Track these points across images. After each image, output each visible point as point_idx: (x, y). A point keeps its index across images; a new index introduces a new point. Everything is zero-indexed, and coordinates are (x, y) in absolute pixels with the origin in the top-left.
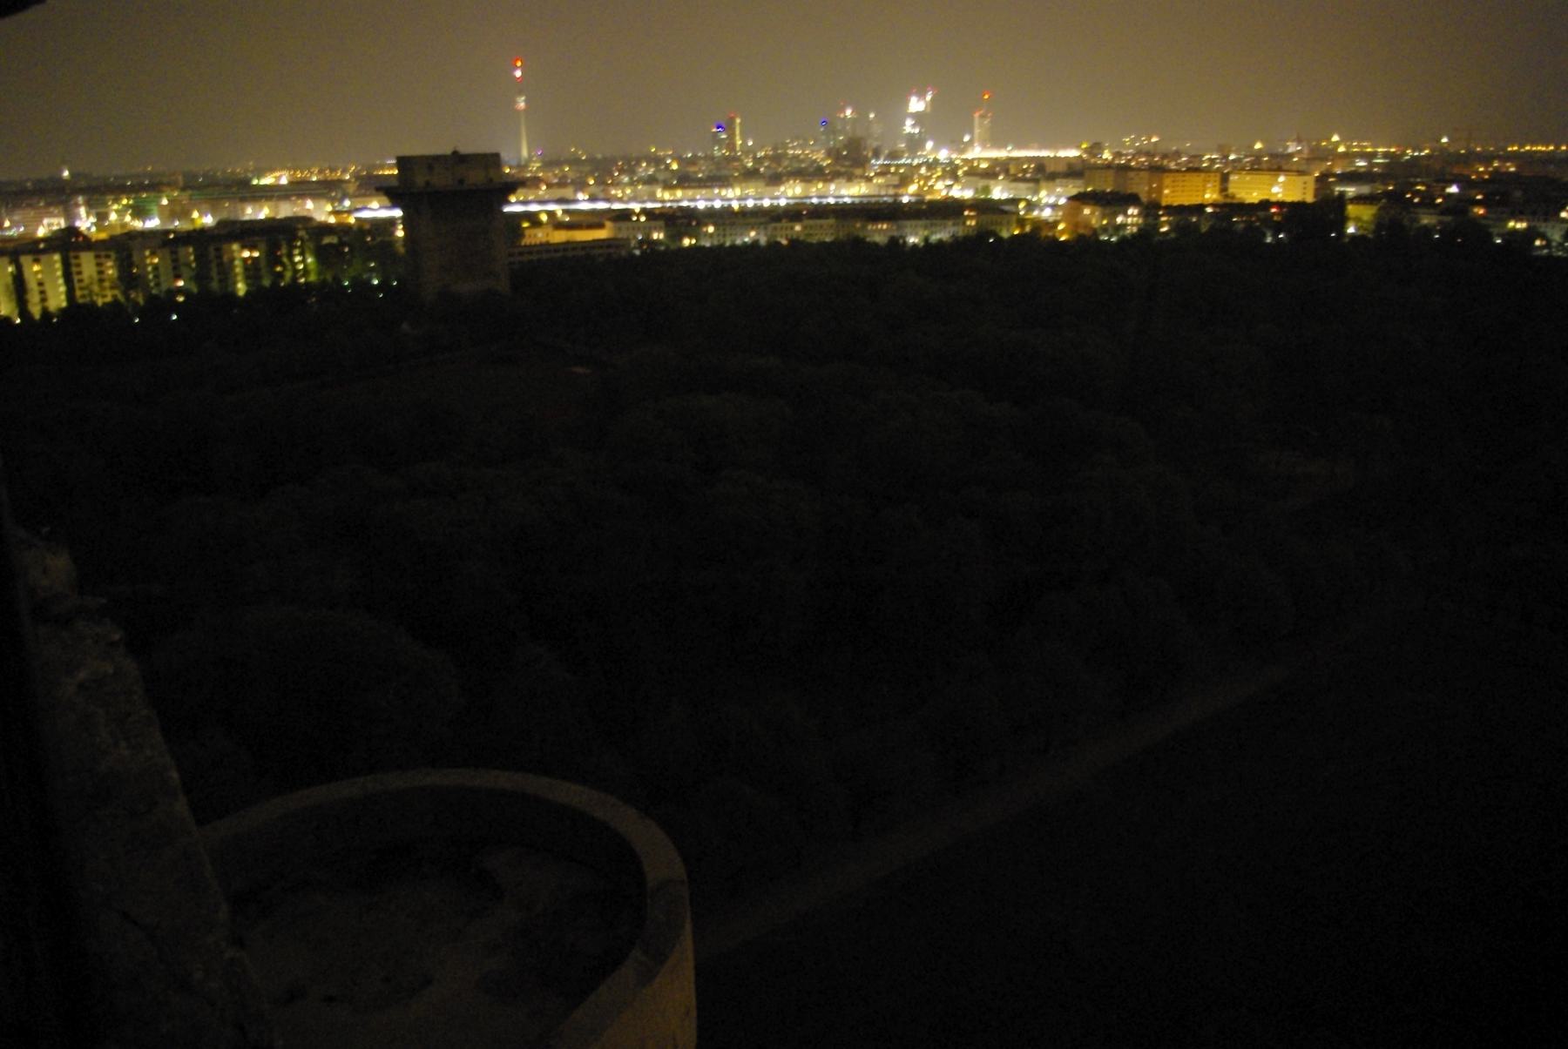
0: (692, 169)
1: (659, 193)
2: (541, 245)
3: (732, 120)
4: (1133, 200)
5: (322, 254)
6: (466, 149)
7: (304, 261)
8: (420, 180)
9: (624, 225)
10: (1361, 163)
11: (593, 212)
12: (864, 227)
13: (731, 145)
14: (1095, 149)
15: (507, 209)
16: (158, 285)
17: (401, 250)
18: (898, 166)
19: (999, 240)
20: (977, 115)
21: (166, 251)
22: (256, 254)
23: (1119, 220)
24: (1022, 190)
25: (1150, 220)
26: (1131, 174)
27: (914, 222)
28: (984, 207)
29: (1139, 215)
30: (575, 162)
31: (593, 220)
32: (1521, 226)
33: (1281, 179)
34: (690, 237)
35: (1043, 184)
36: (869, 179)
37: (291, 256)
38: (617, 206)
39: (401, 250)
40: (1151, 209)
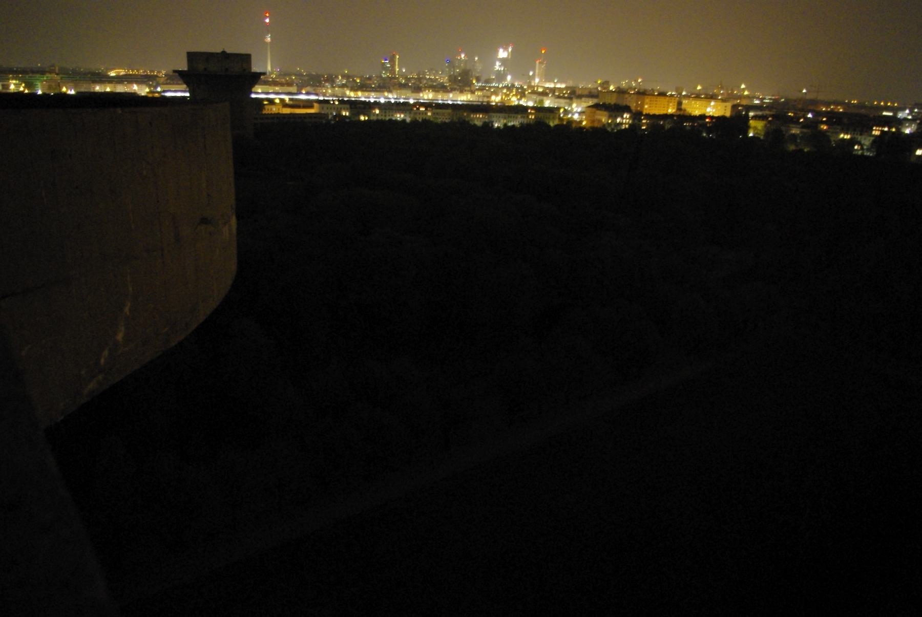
1: (348, 92)
3: (394, 56)
4: (627, 109)
6: (229, 51)
8: (201, 67)
9: (326, 106)
10: (757, 102)
12: (468, 116)
13: (392, 71)
14: (606, 84)
15: (253, 96)
18: (490, 87)
20: (537, 62)
23: (618, 120)
24: (561, 103)
27: (498, 115)
28: (539, 109)
29: (630, 118)
30: (299, 75)
31: (308, 104)
32: (847, 137)
33: (712, 103)
34: (364, 115)
35: (574, 100)
36: (473, 92)
38: (321, 98)
40: (637, 115)
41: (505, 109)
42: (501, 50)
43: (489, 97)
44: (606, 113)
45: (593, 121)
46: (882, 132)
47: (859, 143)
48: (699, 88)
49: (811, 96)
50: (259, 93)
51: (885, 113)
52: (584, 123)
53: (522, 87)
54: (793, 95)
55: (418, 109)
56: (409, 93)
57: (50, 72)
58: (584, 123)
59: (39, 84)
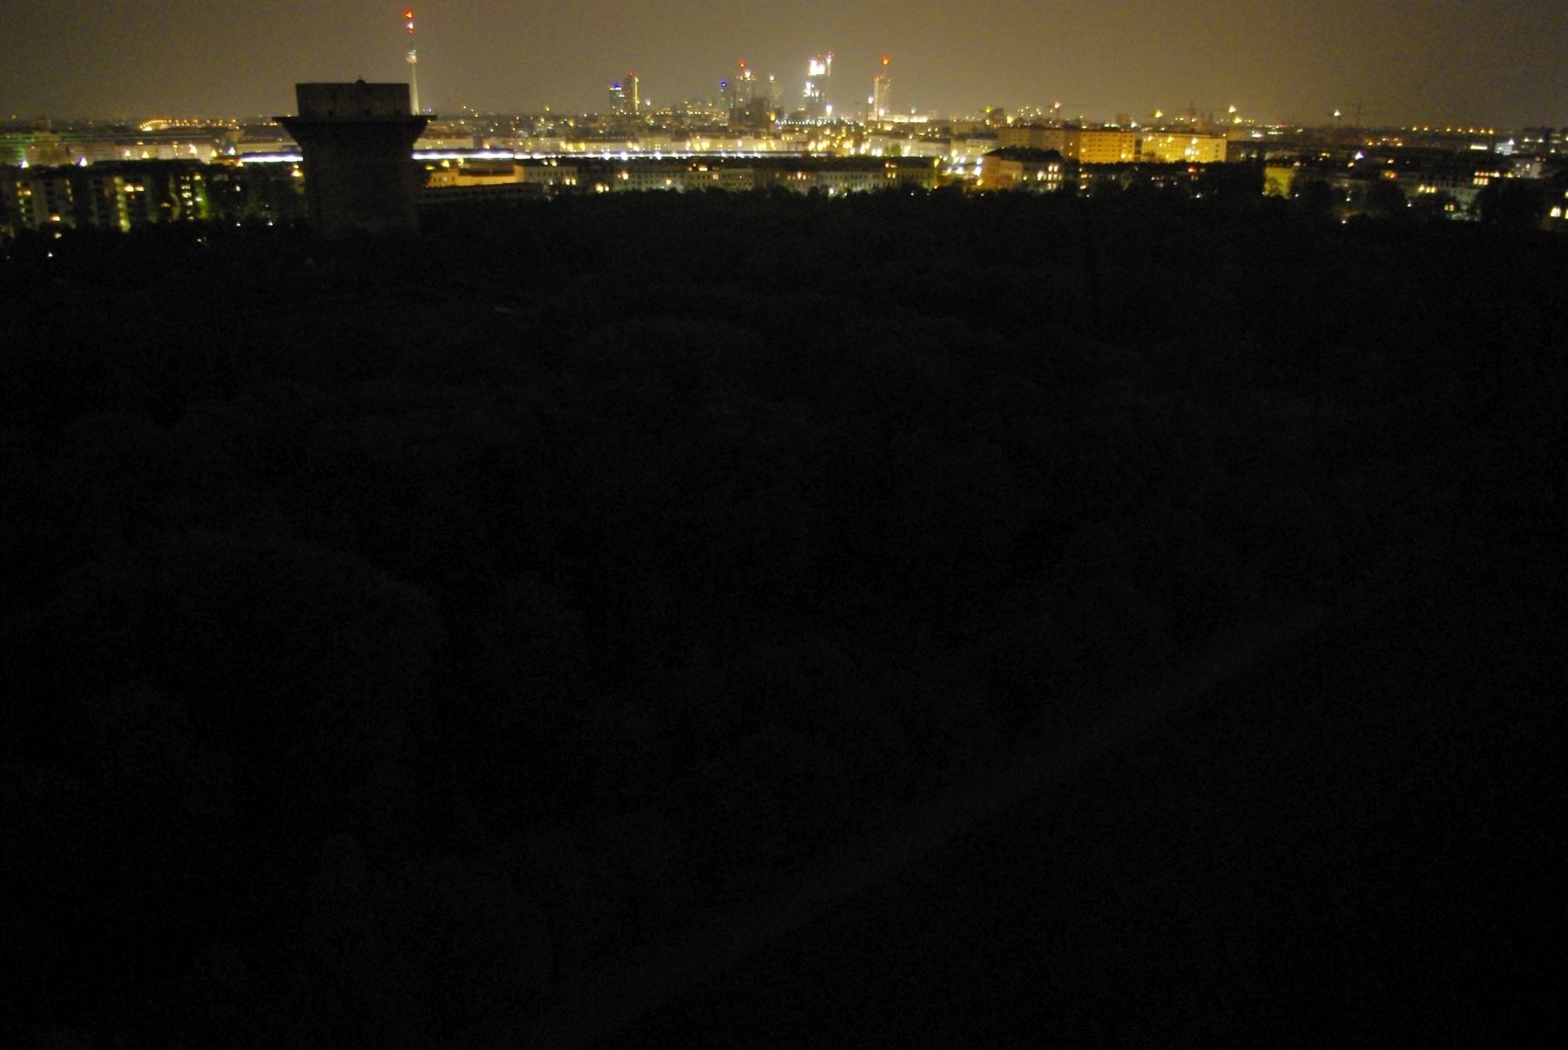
0: (592, 125)
1: (563, 145)
2: (448, 188)
4: (1053, 156)
5: (213, 190)
6: (371, 79)
7: (192, 198)
9: (534, 169)
10: (1257, 135)
11: (496, 161)
12: (783, 177)
13: (629, 105)
14: (998, 114)
15: (417, 157)
16: (31, 219)
17: (301, 191)
18: (802, 127)
19: (922, 192)
20: (877, 80)
21: (41, 183)
22: (141, 189)
23: (1040, 176)
24: (930, 150)
25: (1071, 176)
26: (1048, 133)
27: (834, 174)
29: (1059, 171)
33: (1194, 141)
34: (603, 183)
35: (953, 143)
36: (777, 136)
37: (179, 192)
39: (301, 191)
40: (1071, 166)
41: (833, 164)
42: (814, 63)
43: (805, 144)
44: (1019, 164)
45: (998, 181)
46: (1491, 178)
47: (1452, 200)
48: (1159, 115)
49: (1345, 123)
50: (425, 151)
51: (1473, 147)
52: (979, 183)
53: (856, 125)
54: (1317, 121)
55: (696, 169)
56: (669, 144)
57: (38, 129)
58: (979, 183)
59: (23, 151)
